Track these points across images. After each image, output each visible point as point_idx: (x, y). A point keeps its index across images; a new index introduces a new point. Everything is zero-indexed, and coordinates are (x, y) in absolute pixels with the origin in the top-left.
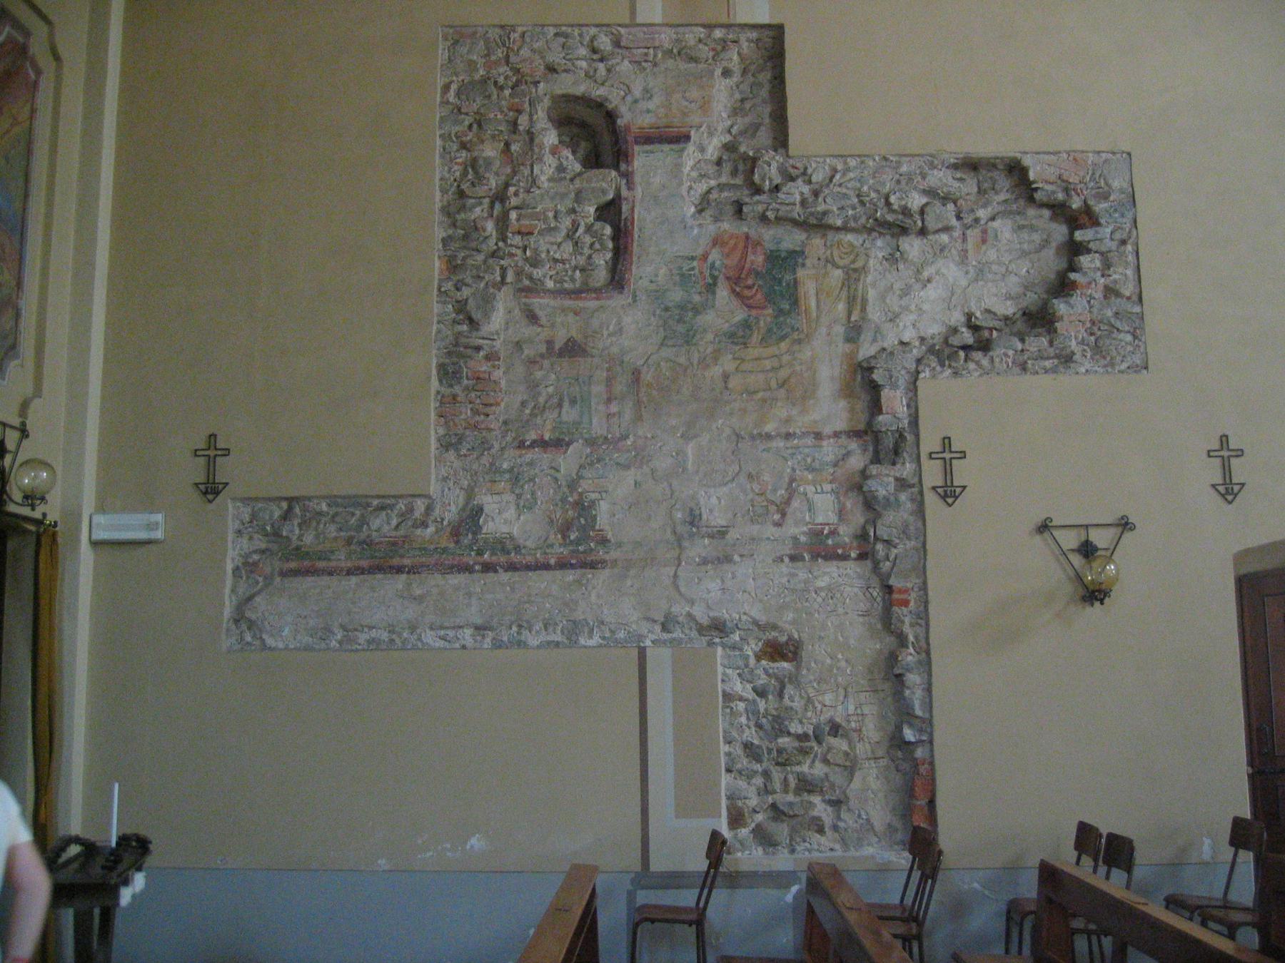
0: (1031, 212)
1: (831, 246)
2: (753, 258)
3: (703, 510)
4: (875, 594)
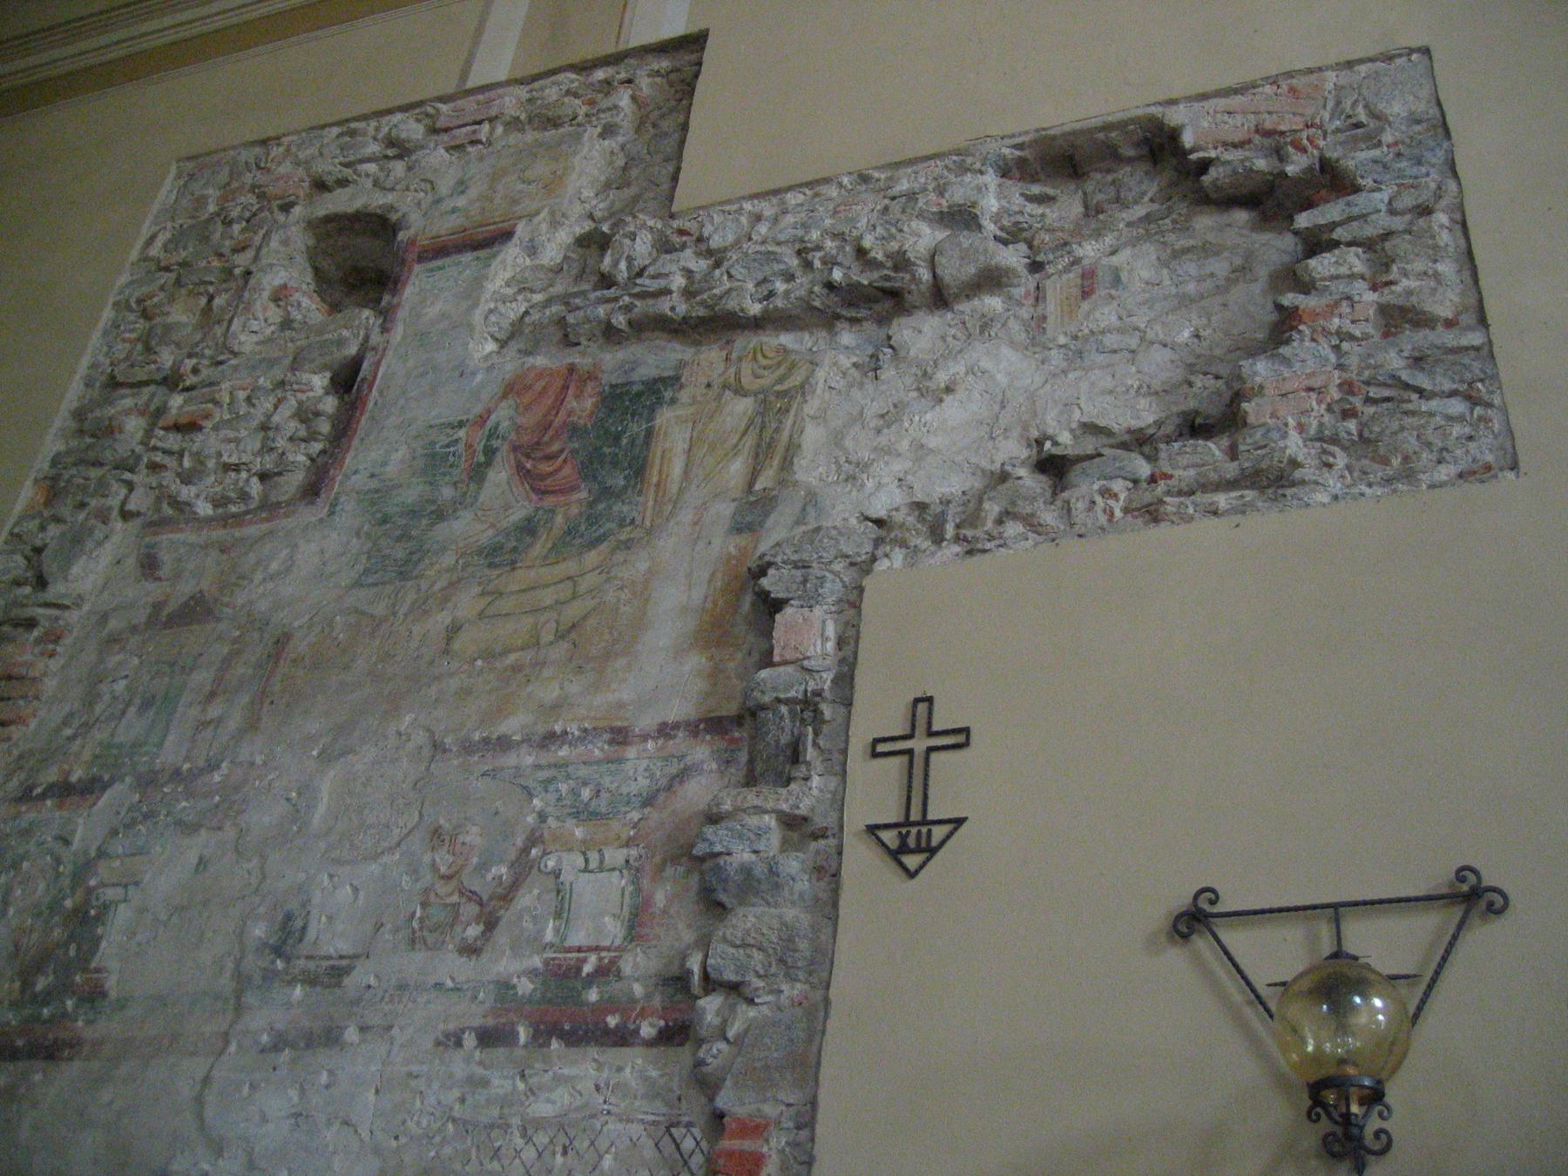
0: (1206, 223)
1: (740, 359)
3: (315, 912)
4: (688, 1144)
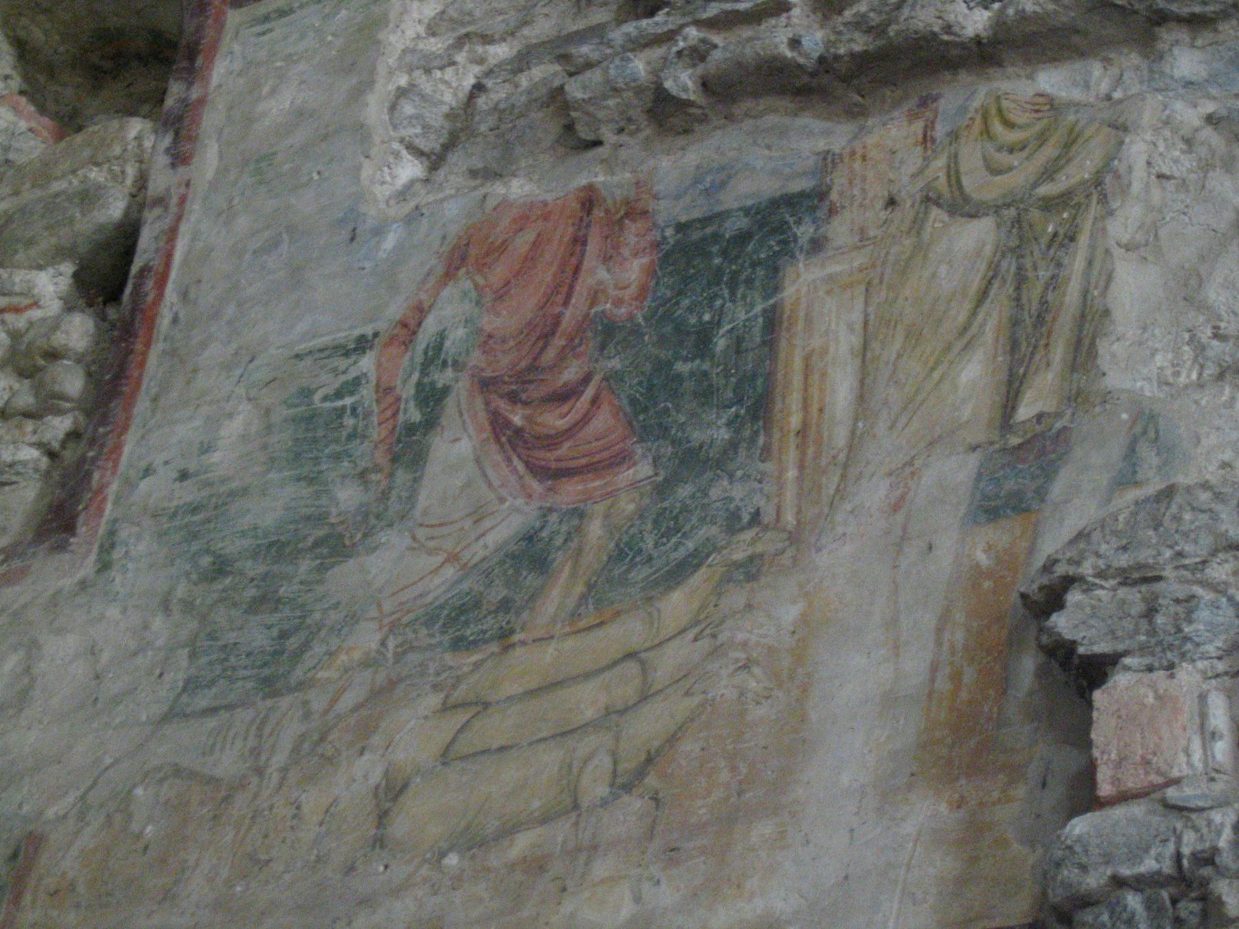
1: (954, 136)
2: (602, 274)
